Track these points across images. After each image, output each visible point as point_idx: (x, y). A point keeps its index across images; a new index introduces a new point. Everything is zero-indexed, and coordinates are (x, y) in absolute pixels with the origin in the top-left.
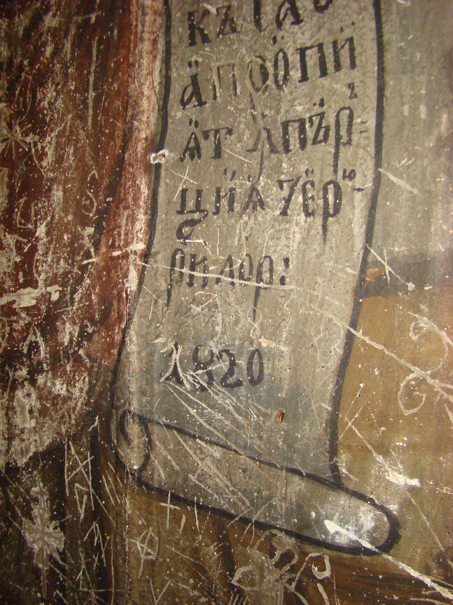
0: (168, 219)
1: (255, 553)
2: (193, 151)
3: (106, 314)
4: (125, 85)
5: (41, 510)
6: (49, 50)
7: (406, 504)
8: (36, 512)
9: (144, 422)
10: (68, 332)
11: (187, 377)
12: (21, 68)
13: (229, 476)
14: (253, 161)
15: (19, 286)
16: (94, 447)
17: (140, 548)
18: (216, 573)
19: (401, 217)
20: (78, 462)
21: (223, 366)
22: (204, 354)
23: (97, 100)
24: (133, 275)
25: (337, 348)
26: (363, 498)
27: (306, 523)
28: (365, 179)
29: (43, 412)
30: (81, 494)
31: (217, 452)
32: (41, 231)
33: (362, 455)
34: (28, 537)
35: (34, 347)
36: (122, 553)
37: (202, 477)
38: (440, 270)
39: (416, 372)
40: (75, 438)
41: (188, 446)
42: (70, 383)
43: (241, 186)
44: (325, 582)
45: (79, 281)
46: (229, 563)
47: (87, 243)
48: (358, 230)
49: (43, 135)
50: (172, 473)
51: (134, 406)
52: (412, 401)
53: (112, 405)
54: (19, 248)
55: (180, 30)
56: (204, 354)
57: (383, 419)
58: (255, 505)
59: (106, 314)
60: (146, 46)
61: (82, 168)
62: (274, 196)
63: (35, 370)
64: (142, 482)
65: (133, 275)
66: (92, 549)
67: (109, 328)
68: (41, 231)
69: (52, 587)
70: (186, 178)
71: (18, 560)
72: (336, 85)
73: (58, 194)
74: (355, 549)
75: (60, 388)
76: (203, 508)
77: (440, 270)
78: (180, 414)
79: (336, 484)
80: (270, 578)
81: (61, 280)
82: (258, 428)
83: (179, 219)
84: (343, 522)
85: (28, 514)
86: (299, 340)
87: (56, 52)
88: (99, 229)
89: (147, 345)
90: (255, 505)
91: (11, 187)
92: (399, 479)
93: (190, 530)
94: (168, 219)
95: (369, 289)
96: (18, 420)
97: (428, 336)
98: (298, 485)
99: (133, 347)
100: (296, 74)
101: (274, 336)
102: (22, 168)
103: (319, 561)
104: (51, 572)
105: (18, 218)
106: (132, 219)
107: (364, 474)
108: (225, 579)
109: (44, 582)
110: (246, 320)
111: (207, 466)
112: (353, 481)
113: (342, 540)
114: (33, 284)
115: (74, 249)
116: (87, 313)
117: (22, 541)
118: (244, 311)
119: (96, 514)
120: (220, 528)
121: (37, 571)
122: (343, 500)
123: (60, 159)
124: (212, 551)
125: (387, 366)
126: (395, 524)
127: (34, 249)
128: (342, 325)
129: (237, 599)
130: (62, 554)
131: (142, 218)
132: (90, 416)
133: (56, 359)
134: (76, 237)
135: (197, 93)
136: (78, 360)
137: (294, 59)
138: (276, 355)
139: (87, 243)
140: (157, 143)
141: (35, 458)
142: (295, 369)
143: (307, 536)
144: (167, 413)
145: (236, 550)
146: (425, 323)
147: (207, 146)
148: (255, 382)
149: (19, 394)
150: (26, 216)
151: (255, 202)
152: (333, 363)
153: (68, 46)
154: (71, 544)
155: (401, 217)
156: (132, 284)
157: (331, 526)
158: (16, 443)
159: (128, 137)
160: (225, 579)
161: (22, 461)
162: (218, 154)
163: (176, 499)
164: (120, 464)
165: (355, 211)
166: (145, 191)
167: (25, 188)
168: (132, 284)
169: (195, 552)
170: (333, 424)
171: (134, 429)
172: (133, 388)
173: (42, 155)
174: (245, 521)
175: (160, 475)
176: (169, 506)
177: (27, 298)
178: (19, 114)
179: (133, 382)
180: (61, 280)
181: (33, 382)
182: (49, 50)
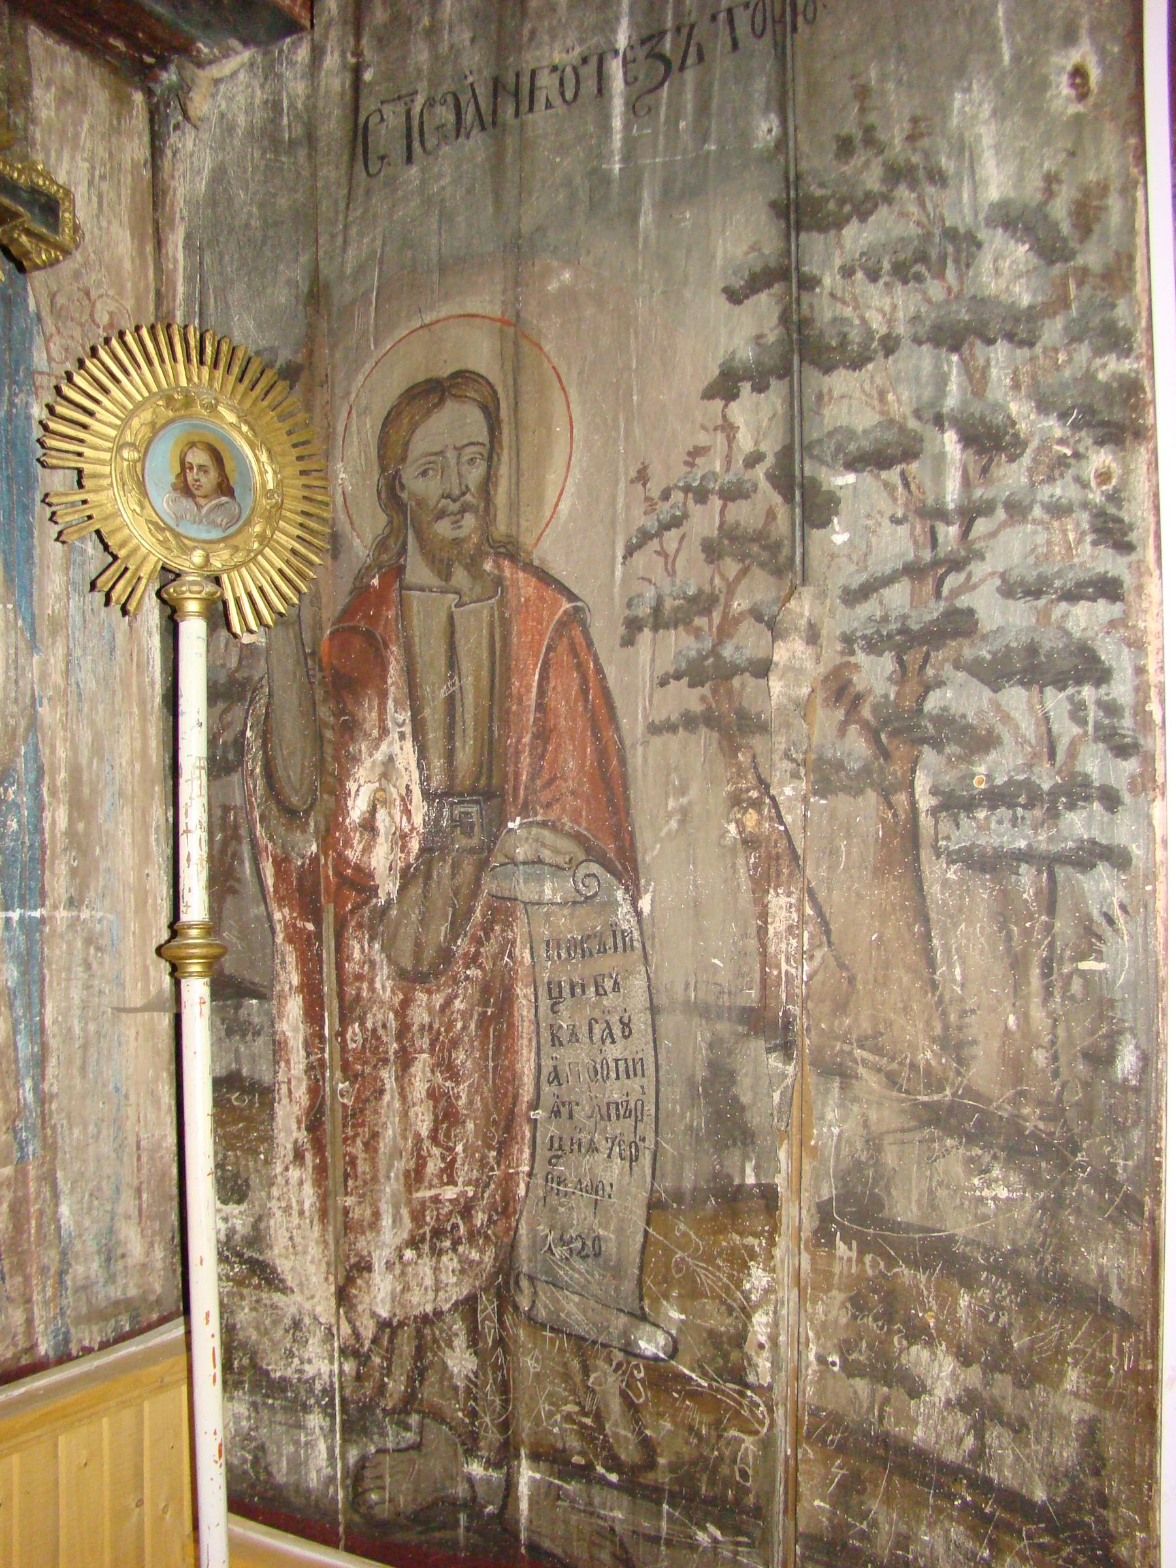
0: (542, 1152)
1: (600, 1363)
2: (557, 1113)
3: (505, 1208)
4: (512, 1064)
5: (460, 1342)
6: (459, 1025)
7: (680, 1330)
8: (456, 1343)
9: (532, 1279)
10: (480, 1218)
11: (558, 1251)
12: (439, 1033)
13: (584, 1312)
14: (590, 1124)
15: (443, 1184)
16: (499, 1296)
17: (530, 1364)
18: (578, 1379)
19: (669, 1167)
20: (487, 1306)
21: (578, 1245)
22: (567, 1237)
23: (495, 1068)
24: (522, 1186)
25: (640, 1238)
26: (657, 1326)
27: (628, 1343)
28: (650, 1143)
29: (463, 1271)
30: (490, 1330)
31: (576, 1298)
32: (459, 1148)
33: (655, 1302)
34: (450, 1363)
35: (455, 1227)
36: (518, 1369)
37: (568, 1314)
38: (688, 1197)
39: (679, 1254)
40: (486, 1290)
41: (559, 1294)
42: (482, 1252)
43: (585, 1137)
44: (642, 1381)
45: (487, 1185)
46: (586, 1370)
47: (493, 1162)
48: (648, 1171)
49: (458, 1083)
50: (550, 1312)
51: (525, 1269)
52: (679, 1270)
53: (511, 1267)
54: (443, 1158)
55: (546, 1035)
56: (567, 1237)
57: (665, 1280)
58: (600, 1332)
59: (505, 1208)
60: (525, 1042)
61: (487, 1113)
62: (604, 1146)
63: (456, 1243)
64: (531, 1318)
65: (522, 1186)
66: (497, 1367)
67: (508, 1217)
68: (459, 1148)
69: (467, 1399)
70: (553, 1130)
71: (441, 1381)
72: (635, 1084)
73: (470, 1126)
74: (656, 1358)
75: (474, 1255)
76: (569, 1335)
77: (688, 1197)
78: (555, 1275)
79: (643, 1318)
80: (610, 1379)
81: (476, 1183)
82: (599, 1283)
83: (549, 1154)
84: (649, 1341)
85: (450, 1345)
86: (620, 1231)
87: (464, 1028)
88: (499, 1153)
89: (533, 1230)
90: (600, 1332)
91: (436, 1115)
92: (675, 1315)
93: (561, 1350)
94: (542, 1152)
95: (654, 1206)
96: (443, 1277)
97: (684, 1234)
98: (623, 1319)
99: (523, 1231)
100: (613, 1075)
101: (606, 1228)
102: (443, 1103)
103: (637, 1367)
104: (468, 1389)
105: (441, 1137)
106: (521, 1151)
107: (658, 1313)
108: (584, 1382)
109: (462, 1395)
110: (591, 1218)
111: (571, 1307)
112: (652, 1316)
113: (648, 1353)
114: (455, 1184)
115: (483, 1164)
116: (493, 1207)
117: (445, 1366)
118: (589, 1213)
119: (500, 1342)
120: (579, 1348)
121: (455, 1388)
122: (648, 1328)
123: (471, 1103)
124: (575, 1364)
125: (666, 1249)
126: (675, 1342)
127: (454, 1161)
128: (642, 1224)
129: (162, 339)
130: (476, 1374)
131: (527, 1152)
132: (497, 1274)
133: (472, 1236)
134: (484, 1157)
135: (557, 1077)
136: (487, 1237)
137: (612, 1065)
138: (607, 1240)
139: (493, 1162)
140: (535, 1105)
141: (456, 1304)
142: (619, 1244)
143: (630, 1351)
144: (546, 1273)
145: (590, 1362)
146: (682, 1227)
147: (564, 1111)
148: (597, 1255)
149: (445, 1258)
150: (447, 1136)
151: (593, 1148)
152: (638, 1246)
153: (473, 1026)
154: (482, 1366)
155: (669, 1167)
156: (521, 1191)
157: (642, 1344)
158: (441, 1294)
159: (516, 1097)
160: (584, 1382)
161: (446, 1307)
162: (571, 1117)
163: (552, 1329)
164: (516, 1308)
165: (646, 1160)
166: (528, 1134)
167: (446, 1116)
168: (521, 1191)
169: (565, 1365)
170: (640, 1282)
171: (524, 1283)
172: (524, 1257)
173: (458, 1097)
174: (594, 1342)
175: (542, 1314)
176: (548, 1334)
177: (450, 1193)
178: (439, 1065)
179: (523, 1252)
180: (476, 1183)
181: (455, 1250)
182: (459, 1025)
